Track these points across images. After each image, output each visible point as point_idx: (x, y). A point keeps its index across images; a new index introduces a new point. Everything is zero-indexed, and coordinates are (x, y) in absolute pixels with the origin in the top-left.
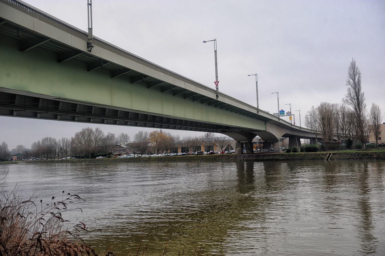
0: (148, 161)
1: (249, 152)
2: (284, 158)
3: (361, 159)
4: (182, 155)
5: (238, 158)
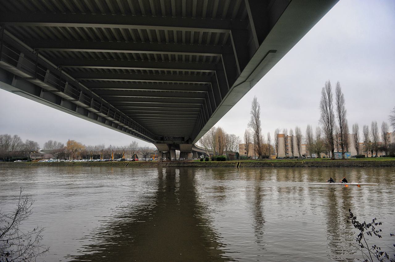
0: (73, 165)
1: (169, 160)
2: (202, 165)
3: (263, 166)
4: (106, 161)
5: (161, 164)
